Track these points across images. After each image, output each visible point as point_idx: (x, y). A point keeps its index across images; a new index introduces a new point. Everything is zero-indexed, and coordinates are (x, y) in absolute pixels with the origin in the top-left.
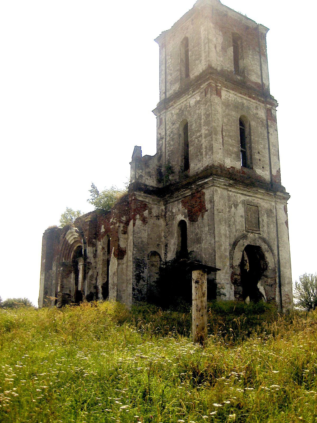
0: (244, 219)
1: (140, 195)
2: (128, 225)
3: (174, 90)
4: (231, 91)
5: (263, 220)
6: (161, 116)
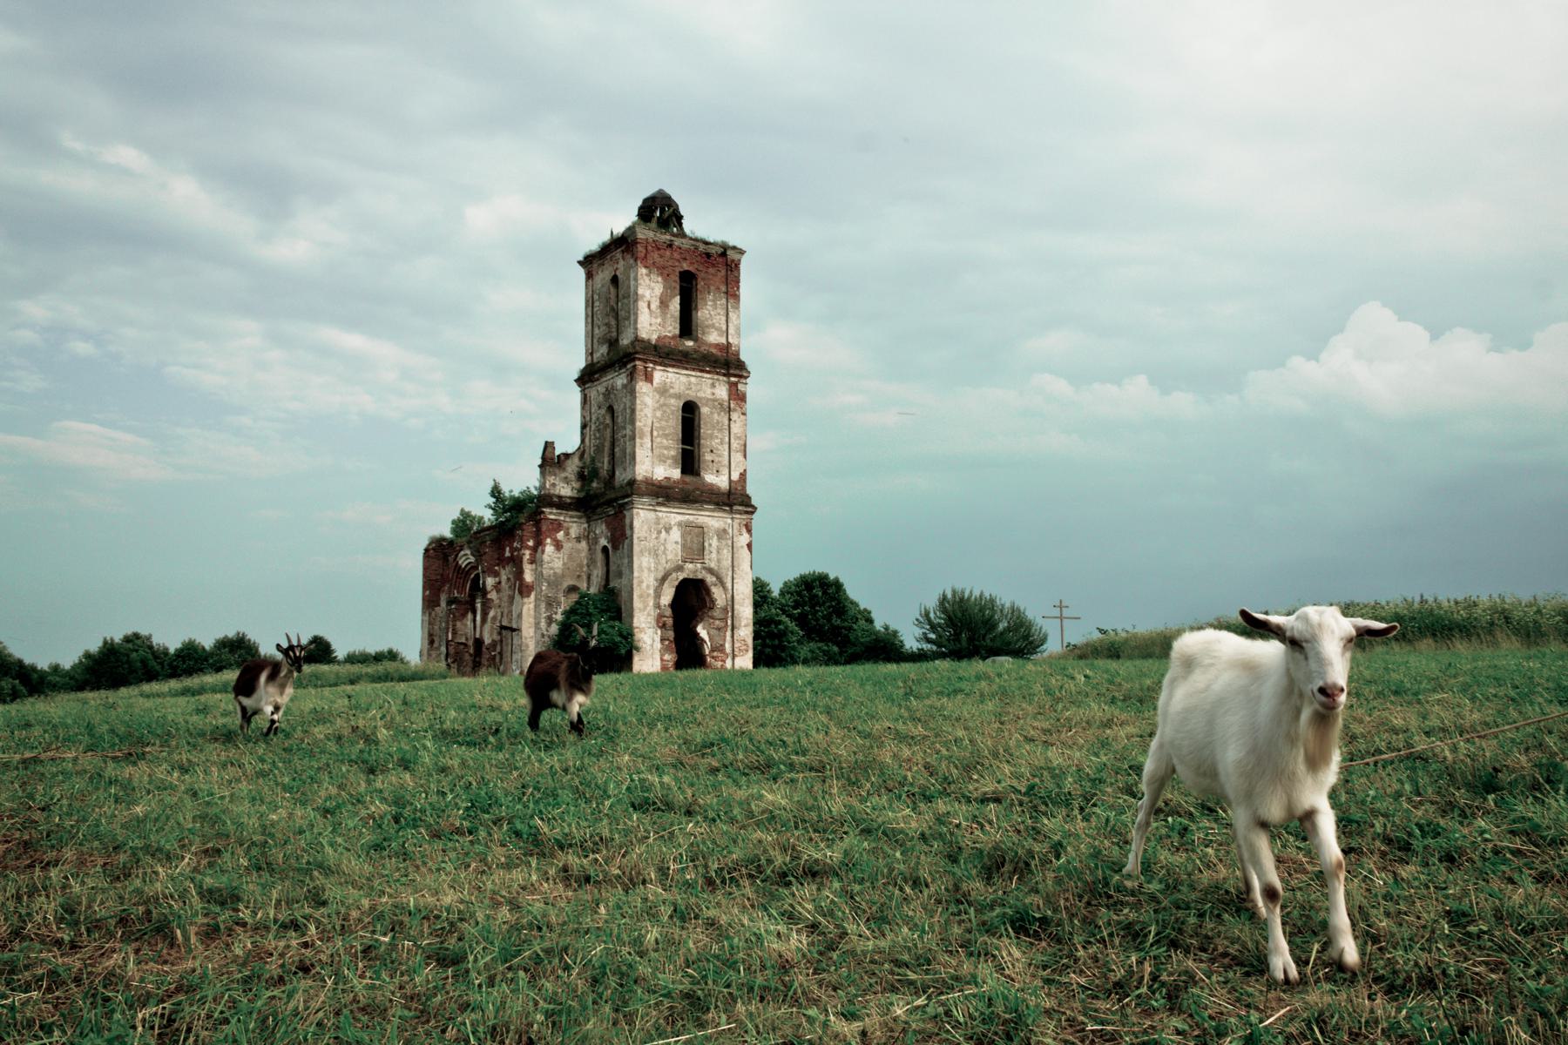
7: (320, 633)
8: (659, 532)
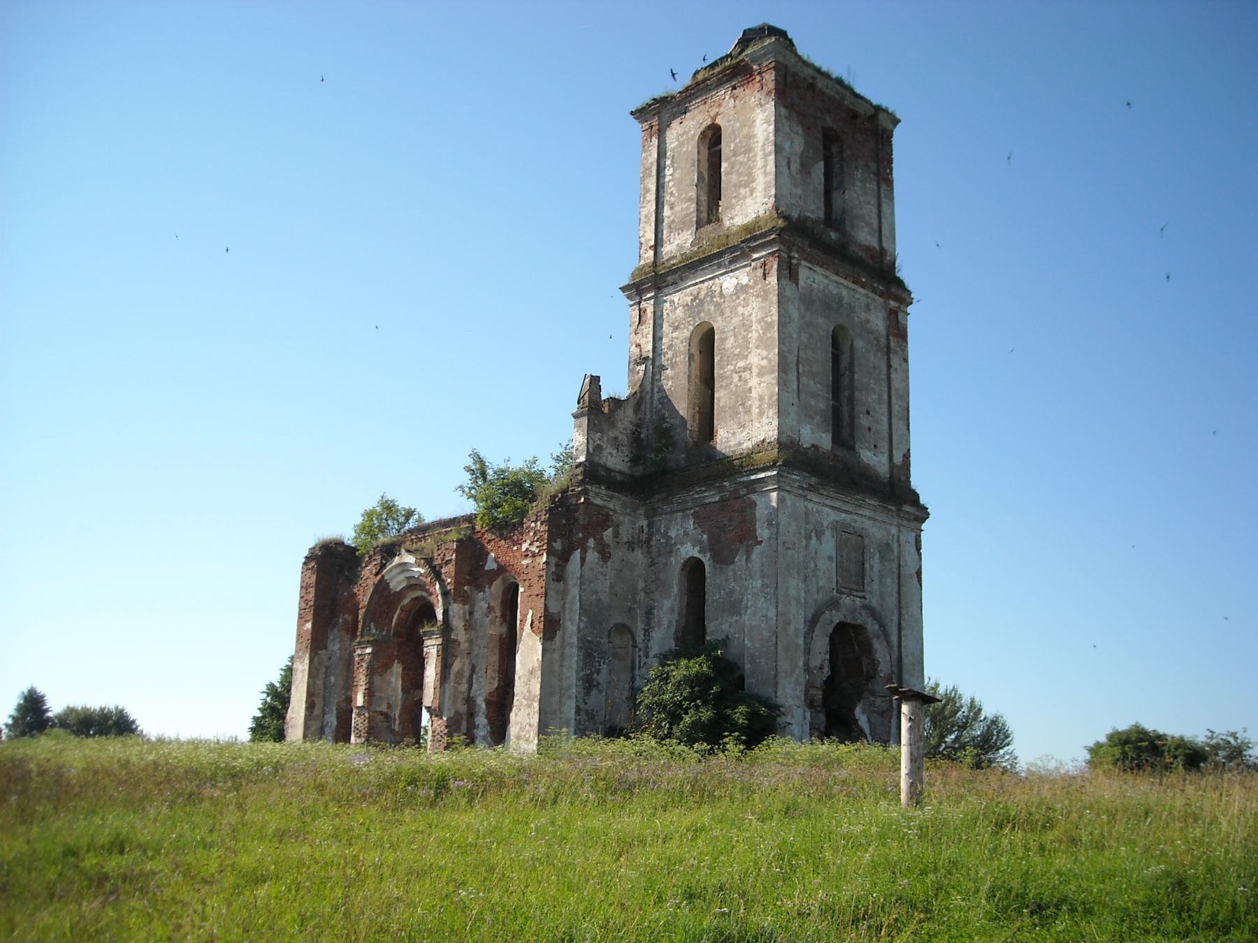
0: (834, 565)
1: (597, 494)
2: (567, 560)
3: (680, 247)
4: (817, 268)
5: (871, 568)
6: (643, 304)
7: (41, 689)
8: (808, 538)
